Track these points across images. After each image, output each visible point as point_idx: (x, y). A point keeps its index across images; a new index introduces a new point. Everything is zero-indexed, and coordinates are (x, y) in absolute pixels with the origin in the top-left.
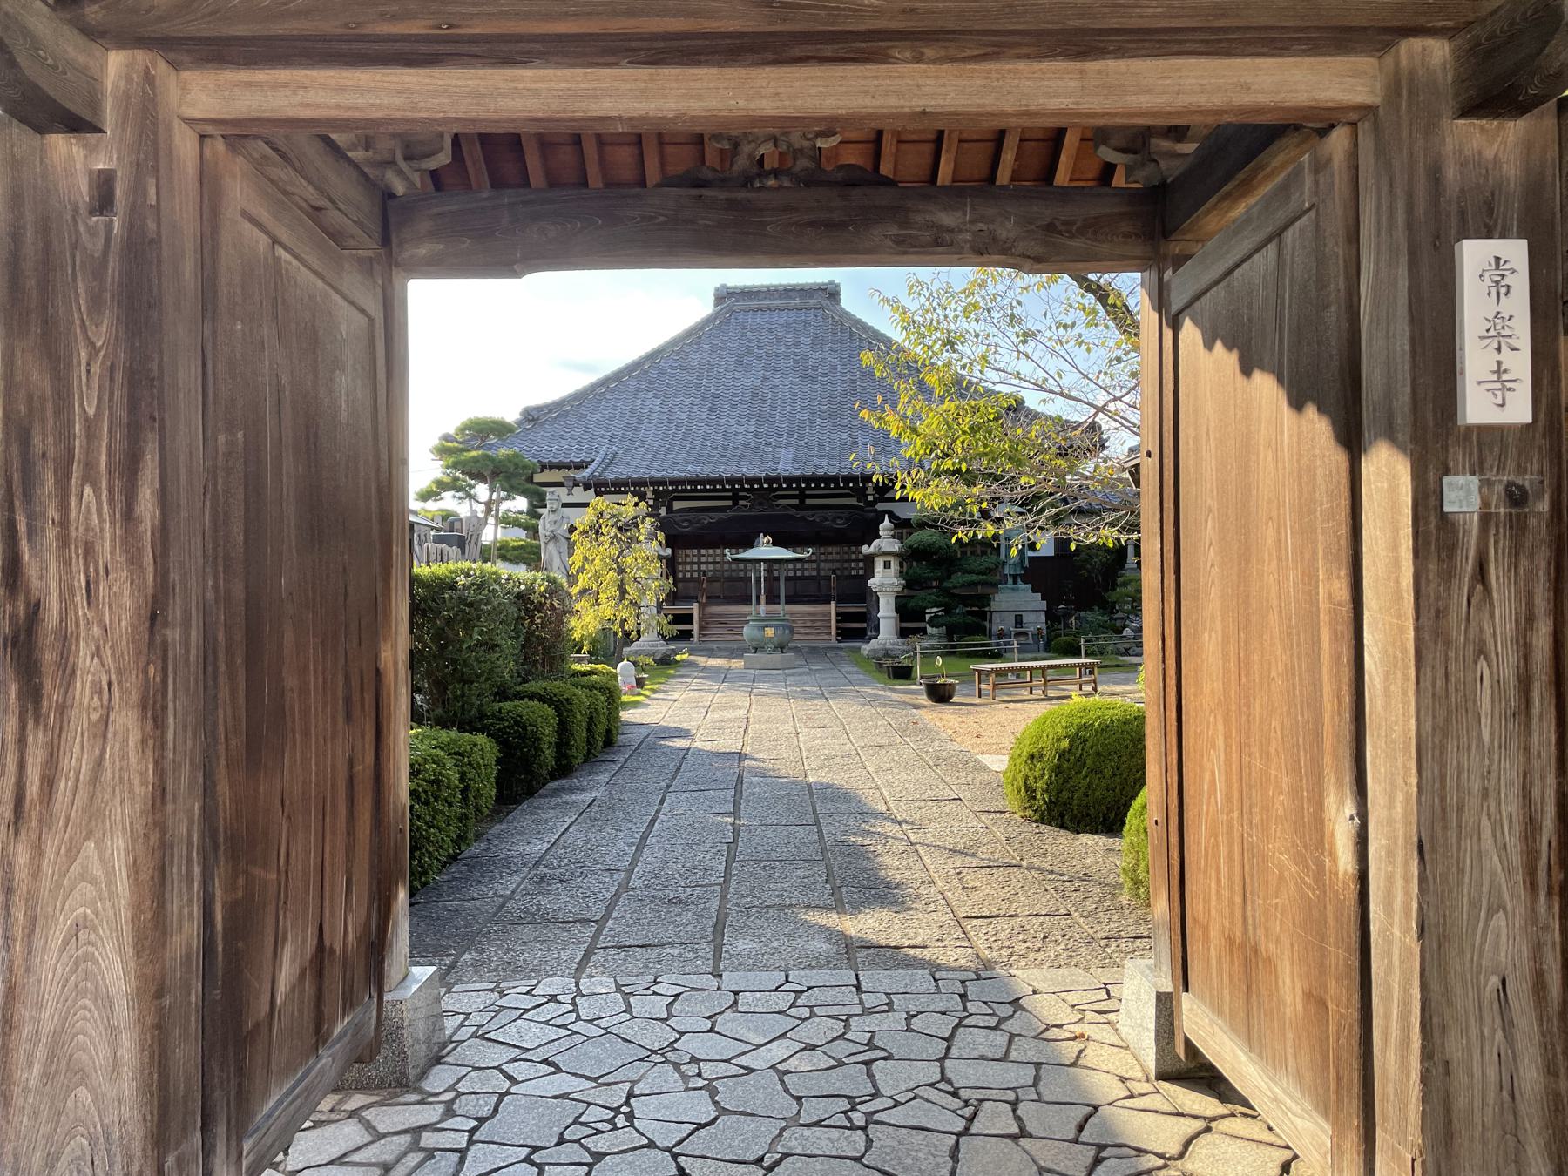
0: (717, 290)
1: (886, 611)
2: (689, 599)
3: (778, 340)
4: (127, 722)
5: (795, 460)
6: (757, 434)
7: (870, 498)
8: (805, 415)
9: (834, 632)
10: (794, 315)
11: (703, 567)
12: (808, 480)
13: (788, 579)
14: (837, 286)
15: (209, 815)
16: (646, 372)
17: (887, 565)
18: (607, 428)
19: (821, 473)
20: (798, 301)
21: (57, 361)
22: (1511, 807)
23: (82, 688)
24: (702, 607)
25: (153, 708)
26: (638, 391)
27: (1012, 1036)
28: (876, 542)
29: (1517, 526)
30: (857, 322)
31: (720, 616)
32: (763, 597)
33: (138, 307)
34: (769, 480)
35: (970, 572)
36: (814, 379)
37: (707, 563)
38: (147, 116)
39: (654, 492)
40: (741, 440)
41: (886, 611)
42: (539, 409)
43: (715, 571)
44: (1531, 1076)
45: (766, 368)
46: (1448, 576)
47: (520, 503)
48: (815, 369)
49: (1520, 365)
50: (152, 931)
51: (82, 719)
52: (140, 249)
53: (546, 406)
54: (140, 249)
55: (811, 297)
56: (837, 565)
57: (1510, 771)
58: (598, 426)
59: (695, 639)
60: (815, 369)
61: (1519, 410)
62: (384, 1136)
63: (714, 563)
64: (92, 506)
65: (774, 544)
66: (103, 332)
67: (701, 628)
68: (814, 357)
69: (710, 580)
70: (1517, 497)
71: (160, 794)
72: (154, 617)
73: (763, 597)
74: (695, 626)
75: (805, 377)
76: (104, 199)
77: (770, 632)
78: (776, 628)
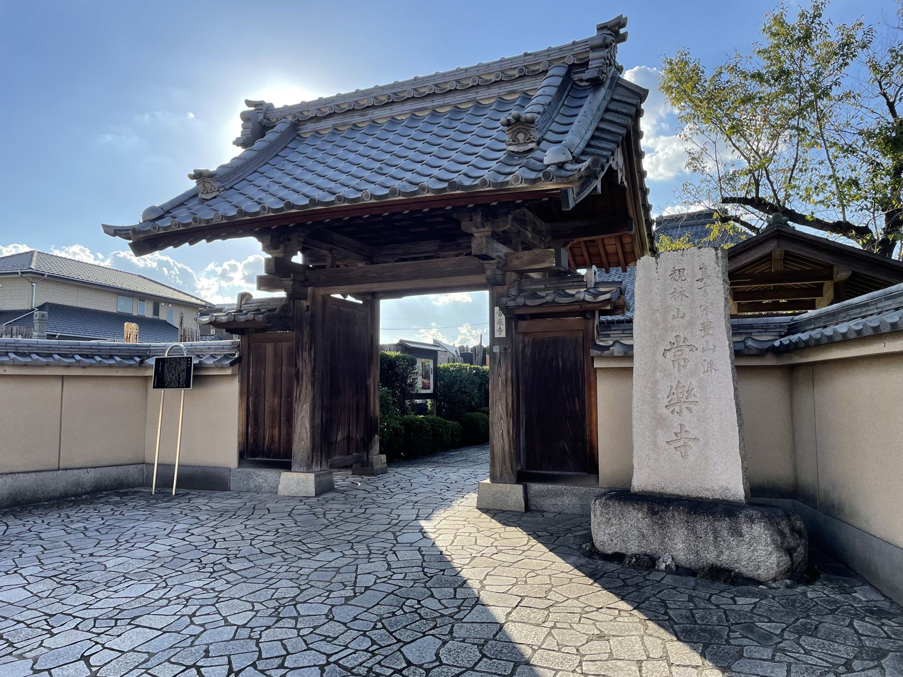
4: (309, 386)
15: (801, 219)
21: (302, 334)
22: (504, 402)
23: (304, 382)
25: (313, 385)
27: (455, 598)
29: (505, 354)
33: (312, 324)
38: (314, 297)
44: (507, 448)
46: (494, 363)
49: (504, 327)
50: (312, 419)
51: (304, 386)
52: (312, 316)
54: (312, 316)
57: (504, 396)
61: (503, 335)
62: (166, 661)
64: (306, 354)
66: (308, 329)
70: (505, 349)
71: (314, 398)
72: (313, 371)
76: (308, 310)
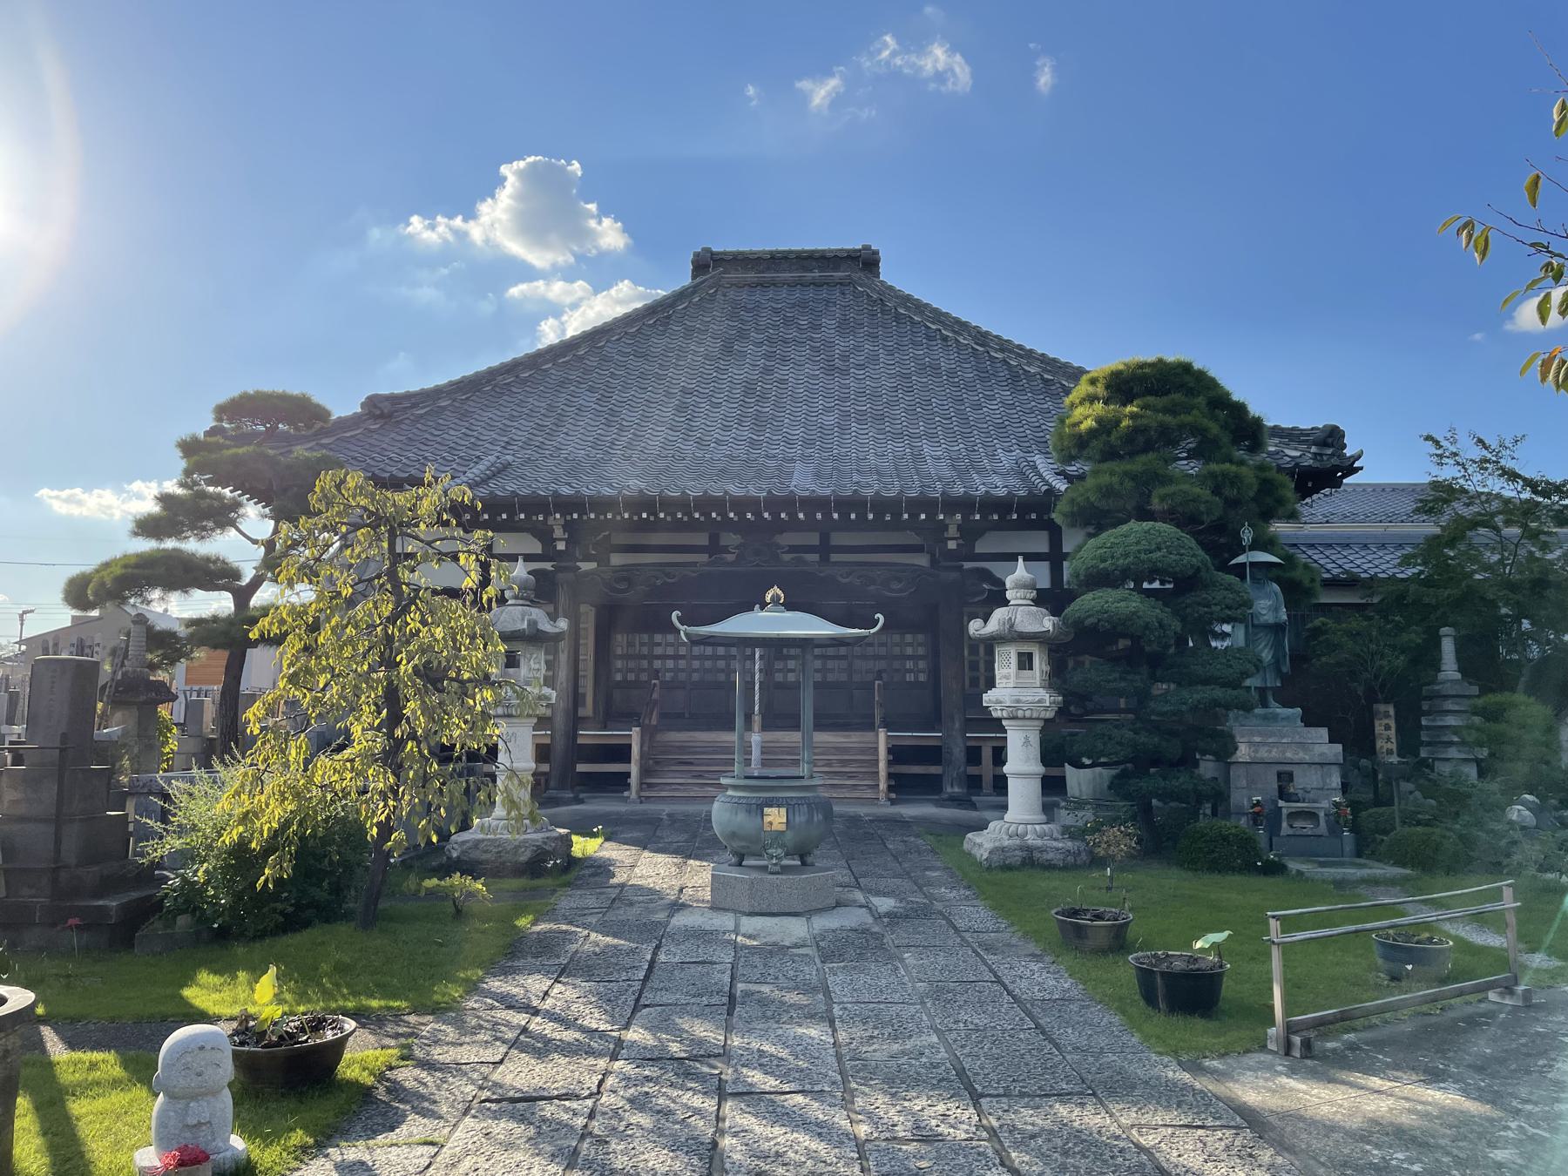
0: (697, 255)
1: (1022, 758)
2: (629, 717)
3: (787, 322)
5: (818, 475)
6: (752, 443)
7: (952, 545)
8: (830, 420)
9: (883, 786)
10: (810, 293)
11: (657, 664)
12: (845, 505)
13: (817, 685)
14: (876, 253)
16: (581, 358)
17: (1025, 662)
18: (504, 431)
19: (869, 493)
20: (817, 274)
24: (648, 734)
26: (562, 384)
28: (999, 614)
30: (906, 300)
31: (682, 749)
32: (757, 719)
34: (774, 503)
35: (1206, 681)
36: (845, 373)
37: (664, 657)
39: (567, 526)
40: (725, 450)
41: (1022, 758)
42: (394, 399)
43: (676, 670)
45: (768, 356)
47: (779, 677)
48: (845, 358)
53: (408, 396)
55: (836, 269)
56: (882, 665)
58: (489, 427)
59: (633, 793)
60: (845, 358)
63: (676, 657)
65: (790, 606)
67: (645, 772)
68: (841, 344)
69: (668, 687)
73: (757, 719)
74: (634, 769)
75: (830, 369)
77: (776, 818)
78: (790, 806)
